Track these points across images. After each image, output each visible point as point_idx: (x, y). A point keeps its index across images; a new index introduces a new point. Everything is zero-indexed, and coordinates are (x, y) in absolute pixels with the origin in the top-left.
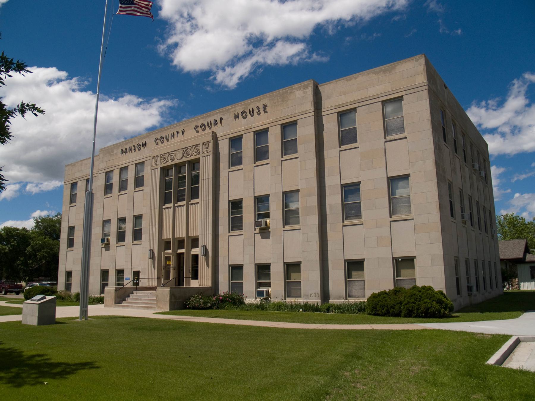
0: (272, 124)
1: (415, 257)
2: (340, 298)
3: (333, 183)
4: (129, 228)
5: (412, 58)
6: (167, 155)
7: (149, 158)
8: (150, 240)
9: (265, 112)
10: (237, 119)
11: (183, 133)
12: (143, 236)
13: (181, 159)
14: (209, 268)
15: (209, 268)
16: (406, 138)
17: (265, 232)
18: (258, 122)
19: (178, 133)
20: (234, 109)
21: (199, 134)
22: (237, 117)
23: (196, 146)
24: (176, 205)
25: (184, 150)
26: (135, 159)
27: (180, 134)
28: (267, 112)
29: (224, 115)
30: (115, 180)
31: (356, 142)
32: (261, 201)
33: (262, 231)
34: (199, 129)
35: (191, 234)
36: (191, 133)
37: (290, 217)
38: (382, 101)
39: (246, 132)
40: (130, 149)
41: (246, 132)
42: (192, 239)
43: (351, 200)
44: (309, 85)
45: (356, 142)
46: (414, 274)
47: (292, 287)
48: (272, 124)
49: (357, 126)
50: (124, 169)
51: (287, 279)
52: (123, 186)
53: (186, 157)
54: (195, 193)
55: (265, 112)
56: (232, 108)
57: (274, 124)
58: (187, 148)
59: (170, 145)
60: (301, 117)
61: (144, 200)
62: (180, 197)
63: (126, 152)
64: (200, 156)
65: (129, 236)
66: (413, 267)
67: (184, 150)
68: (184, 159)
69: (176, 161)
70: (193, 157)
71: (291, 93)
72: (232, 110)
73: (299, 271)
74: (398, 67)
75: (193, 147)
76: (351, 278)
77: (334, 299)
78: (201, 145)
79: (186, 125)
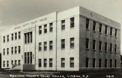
4: (48, 45)
8: (22, 53)
12: (65, 47)
18: (44, 22)
23: (31, 28)
30: (43, 29)
36: (30, 24)
40: (26, 25)
44: (55, 13)
46: (52, 62)
47: (72, 65)
50: (45, 26)
52: (46, 31)
57: (68, 18)
61: (21, 42)
65: (14, 52)
66: (74, 60)
68: (29, 32)
69: (27, 32)
70: (31, 31)
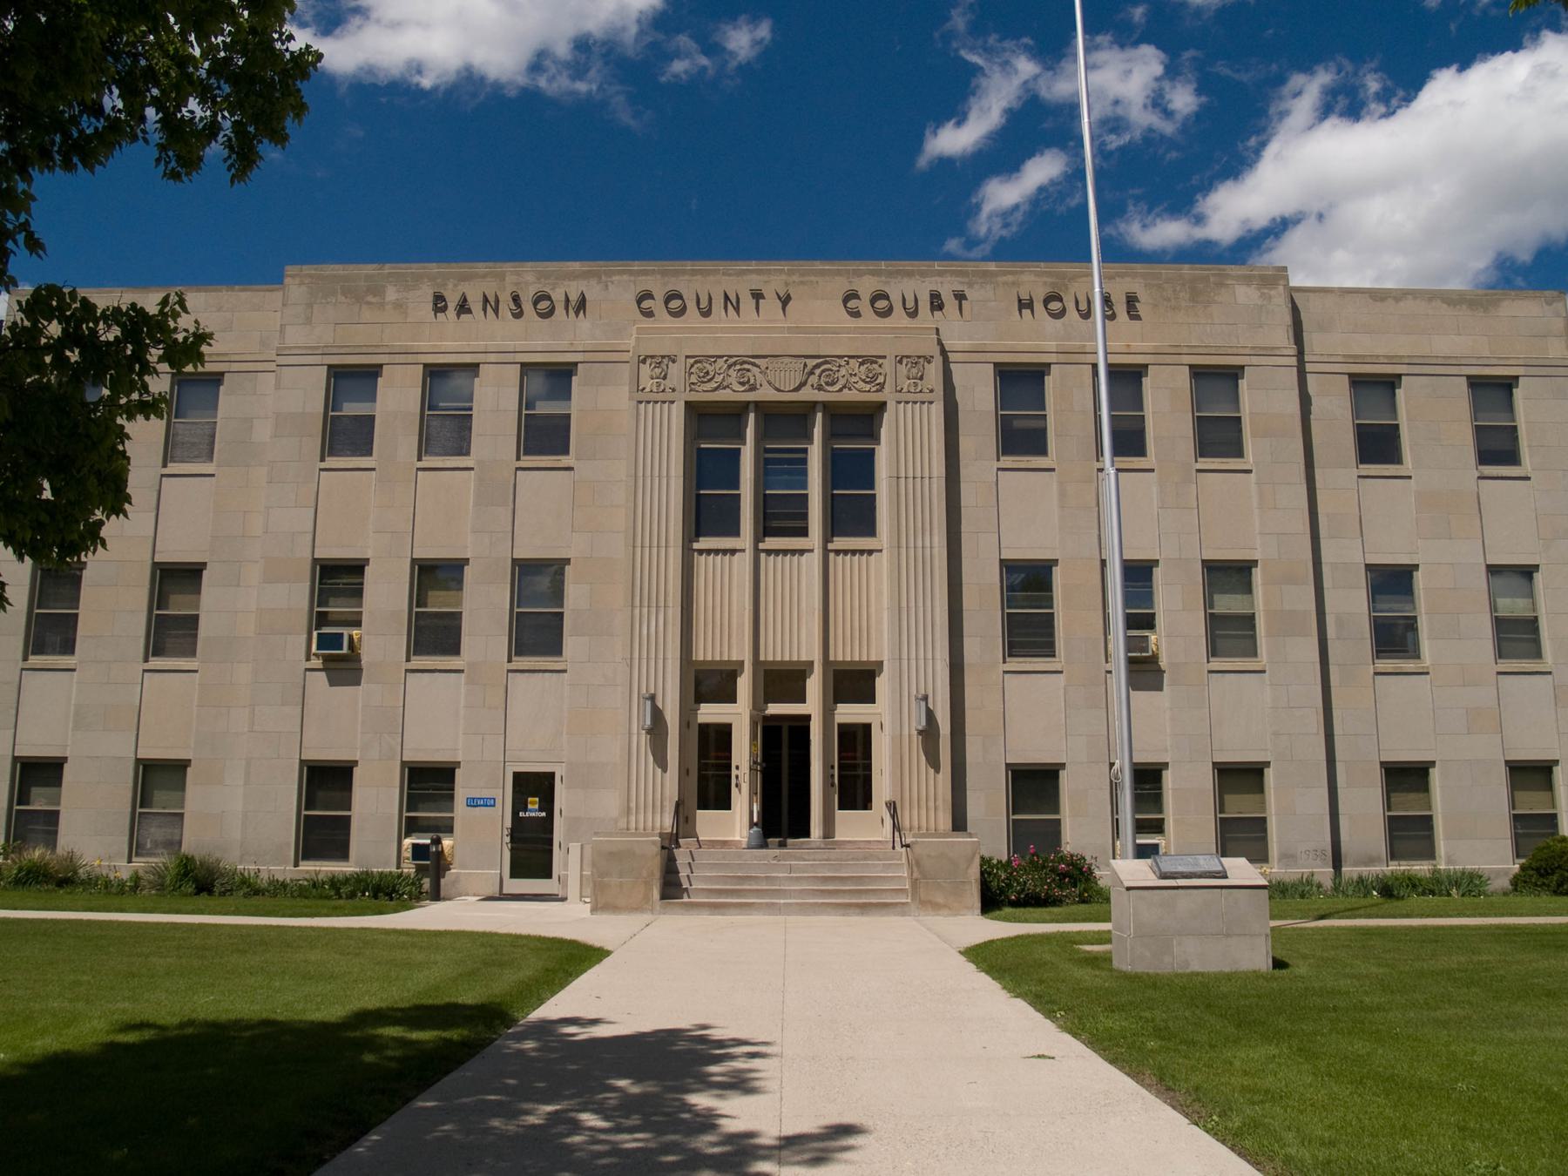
0: (1160, 359)
1: (65, 759)
2: (1371, 861)
3: (1347, 558)
5: (1538, 293)
6: (721, 362)
7: (625, 357)
9: (1133, 314)
10: (1026, 312)
11: (785, 301)
13: (797, 389)
14: (937, 770)
15: (937, 770)
16: (1528, 478)
17: (1144, 671)
19: (758, 296)
20: (1010, 278)
21: (859, 323)
22: (1025, 305)
24: (761, 546)
25: (811, 363)
26: (520, 344)
27: (770, 305)
28: (1138, 318)
29: (971, 285)
31: (566, 451)
32: (436, 575)
33: (332, 665)
34: (656, 304)
35: (769, 654)
37: (1230, 635)
38: (523, 365)
39: (1062, 358)
41: (1062, 358)
42: (698, 672)
43: (438, 603)
45: (566, 451)
48: (1160, 359)
49: (1403, 420)
51: (142, 806)
53: (820, 388)
54: (852, 515)
55: (1133, 314)
56: (1005, 273)
58: (826, 359)
59: (745, 330)
60: (1255, 360)
62: (781, 518)
63: (463, 308)
64: (887, 395)
66: (57, 781)
67: (811, 363)
69: (766, 394)
71: (1221, 285)
72: (1001, 279)
73: (181, 786)
74: (1505, 303)
75: (854, 363)
76: (28, 803)
77: (1356, 864)
78: (888, 365)
79: (795, 278)
